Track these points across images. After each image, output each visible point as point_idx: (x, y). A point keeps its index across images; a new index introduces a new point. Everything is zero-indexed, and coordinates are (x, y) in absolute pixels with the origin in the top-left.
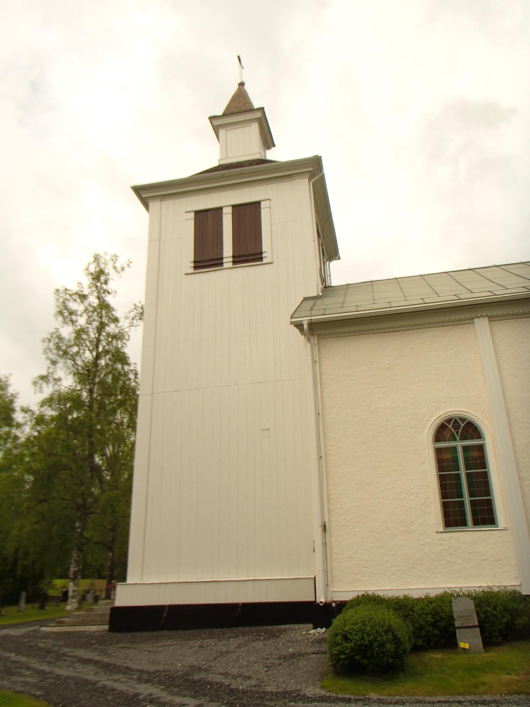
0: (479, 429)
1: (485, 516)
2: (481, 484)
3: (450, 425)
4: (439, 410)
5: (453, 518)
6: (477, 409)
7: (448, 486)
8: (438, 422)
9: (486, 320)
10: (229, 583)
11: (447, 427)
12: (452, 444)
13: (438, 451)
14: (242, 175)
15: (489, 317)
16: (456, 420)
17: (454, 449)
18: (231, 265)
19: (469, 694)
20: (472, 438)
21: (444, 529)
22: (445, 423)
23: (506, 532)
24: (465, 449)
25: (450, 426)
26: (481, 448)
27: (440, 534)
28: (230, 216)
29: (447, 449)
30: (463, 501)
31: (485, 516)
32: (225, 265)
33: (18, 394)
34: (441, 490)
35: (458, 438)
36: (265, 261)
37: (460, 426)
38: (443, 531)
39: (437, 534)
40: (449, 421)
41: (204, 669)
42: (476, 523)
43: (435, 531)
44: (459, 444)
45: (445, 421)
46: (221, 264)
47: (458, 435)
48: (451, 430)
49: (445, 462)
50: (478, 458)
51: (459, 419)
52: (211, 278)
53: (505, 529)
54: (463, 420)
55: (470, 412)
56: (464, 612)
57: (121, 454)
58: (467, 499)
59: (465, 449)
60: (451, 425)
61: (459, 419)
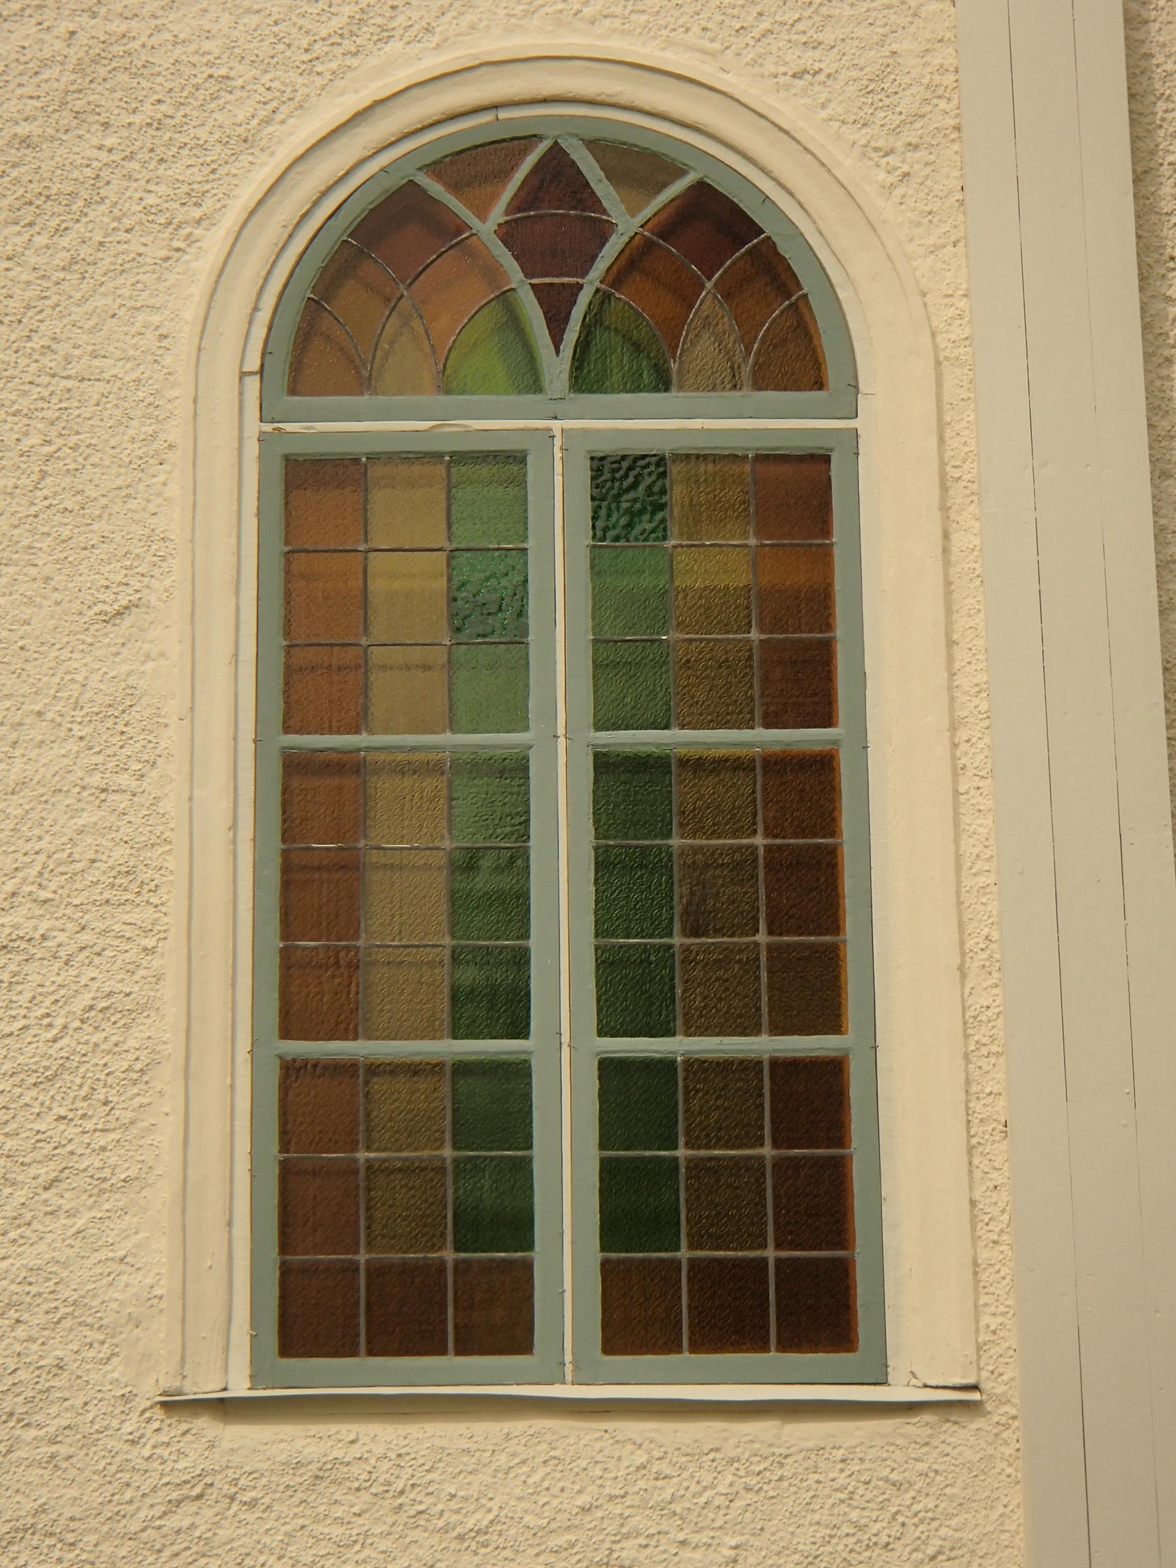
0: (808, 285)
1: (751, 1244)
2: (748, 881)
3: (482, 216)
4: (385, 36)
5: (381, 1263)
6: (809, 59)
8: (357, 166)
11: (448, 231)
12: (489, 422)
16: (556, 153)
17: (509, 463)
21: (255, 1379)
22: (436, 189)
23: (962, 1438)
24: (627, 489)
25: (486, 227)
26: (800, 497)
27: (207, 1426)
30: (517, 1073)
33: (280, 1058)
34: (288, 929)
35: (556, 366)
37: (602, 231)
38: (240, 1388)
39: (173, 1428)
40: (472, 163)
41: (428, 963)
42: (637, 1319)
43: (149, 1390)
44: (567, 431)
45: (435, 168)
47: (557, 343)
48: (492, 273)
50: (752, 614)
51: (592, 145)
53: (962, 1404)
54: (639, 164)
55: (731, 82)
56: (282, 1157)
58: (565, 1050)
59: (627, 489)
60: (498, 214)
61: (592, 145)
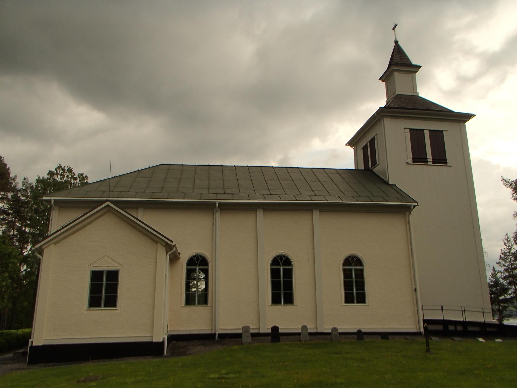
2: (361, 286)
5: (349, 299)
7: (348, 286)
9: (318, 211)
10: (398, 338)
13: (344, 270)
14: (397, 113)
15: (320, 210)
18: (431, 163)
19: (212, 378)
20: (359, 266)
24: (355, 270)
25: (195, 259)
28: (428, 135)
29: (348, 269)
31: (362, 300)
32: (429, 163)
35: (281, 264)
36: (448, 164)
44: (282, 267)
46: (427, 162)
49: (347, 274)
52: (419, 168)
57: (24, 268)
59: (355, 270)
